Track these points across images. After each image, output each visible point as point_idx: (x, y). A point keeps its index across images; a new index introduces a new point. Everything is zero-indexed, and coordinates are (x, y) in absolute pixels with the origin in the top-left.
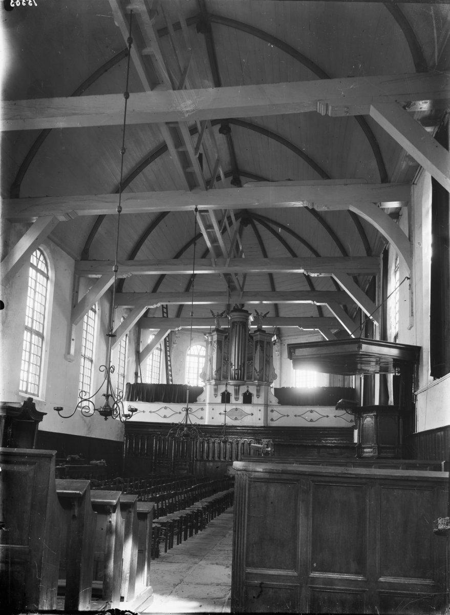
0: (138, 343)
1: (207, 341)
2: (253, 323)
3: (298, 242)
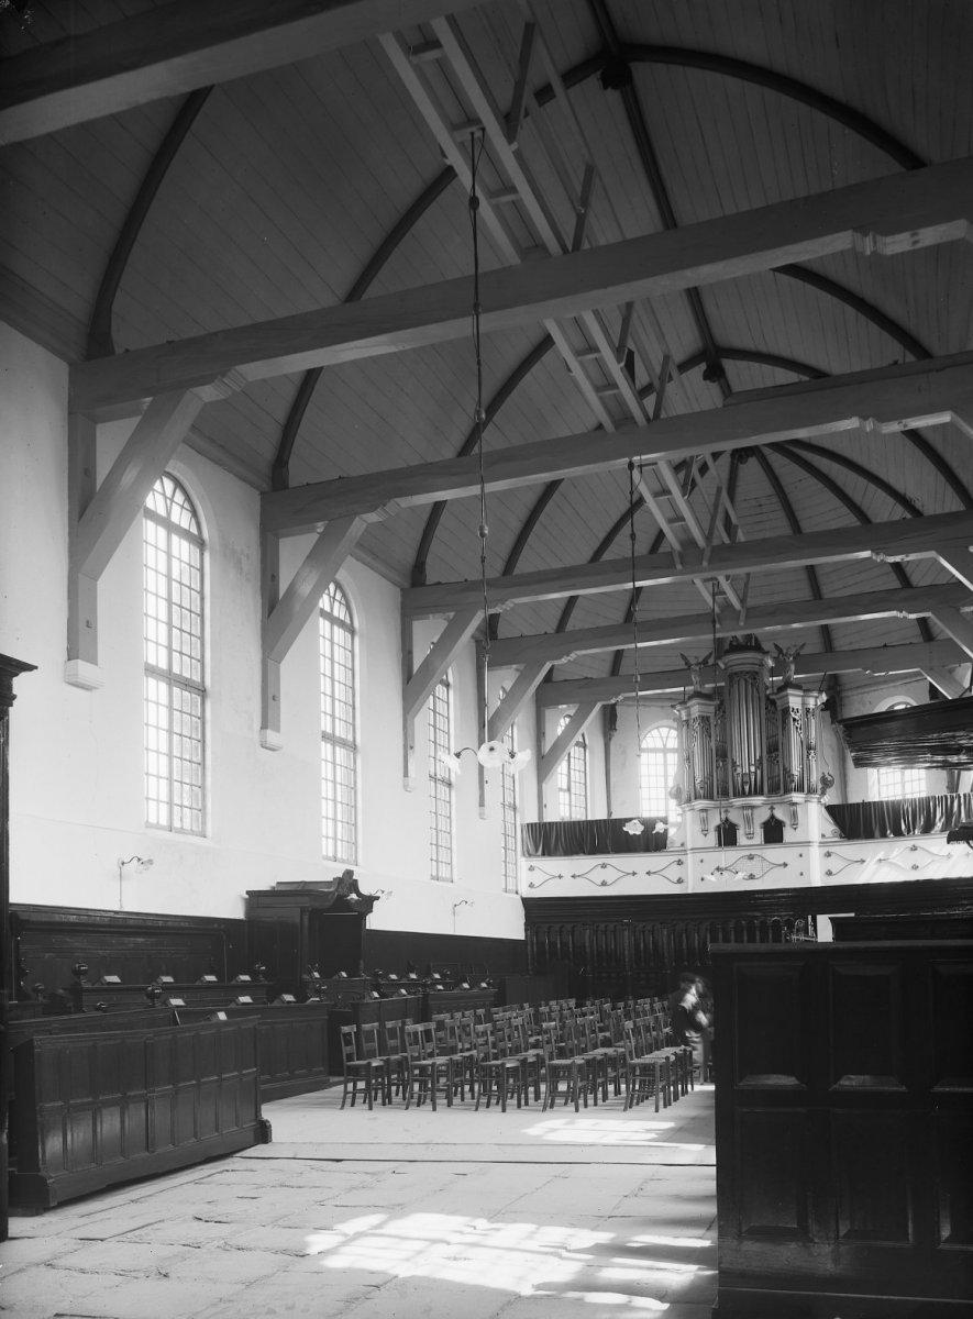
0: (540, 734)
1: (678, 719)
2: (773, 673)
3: (862, 481)
